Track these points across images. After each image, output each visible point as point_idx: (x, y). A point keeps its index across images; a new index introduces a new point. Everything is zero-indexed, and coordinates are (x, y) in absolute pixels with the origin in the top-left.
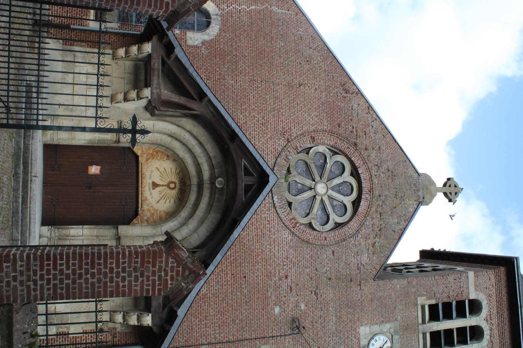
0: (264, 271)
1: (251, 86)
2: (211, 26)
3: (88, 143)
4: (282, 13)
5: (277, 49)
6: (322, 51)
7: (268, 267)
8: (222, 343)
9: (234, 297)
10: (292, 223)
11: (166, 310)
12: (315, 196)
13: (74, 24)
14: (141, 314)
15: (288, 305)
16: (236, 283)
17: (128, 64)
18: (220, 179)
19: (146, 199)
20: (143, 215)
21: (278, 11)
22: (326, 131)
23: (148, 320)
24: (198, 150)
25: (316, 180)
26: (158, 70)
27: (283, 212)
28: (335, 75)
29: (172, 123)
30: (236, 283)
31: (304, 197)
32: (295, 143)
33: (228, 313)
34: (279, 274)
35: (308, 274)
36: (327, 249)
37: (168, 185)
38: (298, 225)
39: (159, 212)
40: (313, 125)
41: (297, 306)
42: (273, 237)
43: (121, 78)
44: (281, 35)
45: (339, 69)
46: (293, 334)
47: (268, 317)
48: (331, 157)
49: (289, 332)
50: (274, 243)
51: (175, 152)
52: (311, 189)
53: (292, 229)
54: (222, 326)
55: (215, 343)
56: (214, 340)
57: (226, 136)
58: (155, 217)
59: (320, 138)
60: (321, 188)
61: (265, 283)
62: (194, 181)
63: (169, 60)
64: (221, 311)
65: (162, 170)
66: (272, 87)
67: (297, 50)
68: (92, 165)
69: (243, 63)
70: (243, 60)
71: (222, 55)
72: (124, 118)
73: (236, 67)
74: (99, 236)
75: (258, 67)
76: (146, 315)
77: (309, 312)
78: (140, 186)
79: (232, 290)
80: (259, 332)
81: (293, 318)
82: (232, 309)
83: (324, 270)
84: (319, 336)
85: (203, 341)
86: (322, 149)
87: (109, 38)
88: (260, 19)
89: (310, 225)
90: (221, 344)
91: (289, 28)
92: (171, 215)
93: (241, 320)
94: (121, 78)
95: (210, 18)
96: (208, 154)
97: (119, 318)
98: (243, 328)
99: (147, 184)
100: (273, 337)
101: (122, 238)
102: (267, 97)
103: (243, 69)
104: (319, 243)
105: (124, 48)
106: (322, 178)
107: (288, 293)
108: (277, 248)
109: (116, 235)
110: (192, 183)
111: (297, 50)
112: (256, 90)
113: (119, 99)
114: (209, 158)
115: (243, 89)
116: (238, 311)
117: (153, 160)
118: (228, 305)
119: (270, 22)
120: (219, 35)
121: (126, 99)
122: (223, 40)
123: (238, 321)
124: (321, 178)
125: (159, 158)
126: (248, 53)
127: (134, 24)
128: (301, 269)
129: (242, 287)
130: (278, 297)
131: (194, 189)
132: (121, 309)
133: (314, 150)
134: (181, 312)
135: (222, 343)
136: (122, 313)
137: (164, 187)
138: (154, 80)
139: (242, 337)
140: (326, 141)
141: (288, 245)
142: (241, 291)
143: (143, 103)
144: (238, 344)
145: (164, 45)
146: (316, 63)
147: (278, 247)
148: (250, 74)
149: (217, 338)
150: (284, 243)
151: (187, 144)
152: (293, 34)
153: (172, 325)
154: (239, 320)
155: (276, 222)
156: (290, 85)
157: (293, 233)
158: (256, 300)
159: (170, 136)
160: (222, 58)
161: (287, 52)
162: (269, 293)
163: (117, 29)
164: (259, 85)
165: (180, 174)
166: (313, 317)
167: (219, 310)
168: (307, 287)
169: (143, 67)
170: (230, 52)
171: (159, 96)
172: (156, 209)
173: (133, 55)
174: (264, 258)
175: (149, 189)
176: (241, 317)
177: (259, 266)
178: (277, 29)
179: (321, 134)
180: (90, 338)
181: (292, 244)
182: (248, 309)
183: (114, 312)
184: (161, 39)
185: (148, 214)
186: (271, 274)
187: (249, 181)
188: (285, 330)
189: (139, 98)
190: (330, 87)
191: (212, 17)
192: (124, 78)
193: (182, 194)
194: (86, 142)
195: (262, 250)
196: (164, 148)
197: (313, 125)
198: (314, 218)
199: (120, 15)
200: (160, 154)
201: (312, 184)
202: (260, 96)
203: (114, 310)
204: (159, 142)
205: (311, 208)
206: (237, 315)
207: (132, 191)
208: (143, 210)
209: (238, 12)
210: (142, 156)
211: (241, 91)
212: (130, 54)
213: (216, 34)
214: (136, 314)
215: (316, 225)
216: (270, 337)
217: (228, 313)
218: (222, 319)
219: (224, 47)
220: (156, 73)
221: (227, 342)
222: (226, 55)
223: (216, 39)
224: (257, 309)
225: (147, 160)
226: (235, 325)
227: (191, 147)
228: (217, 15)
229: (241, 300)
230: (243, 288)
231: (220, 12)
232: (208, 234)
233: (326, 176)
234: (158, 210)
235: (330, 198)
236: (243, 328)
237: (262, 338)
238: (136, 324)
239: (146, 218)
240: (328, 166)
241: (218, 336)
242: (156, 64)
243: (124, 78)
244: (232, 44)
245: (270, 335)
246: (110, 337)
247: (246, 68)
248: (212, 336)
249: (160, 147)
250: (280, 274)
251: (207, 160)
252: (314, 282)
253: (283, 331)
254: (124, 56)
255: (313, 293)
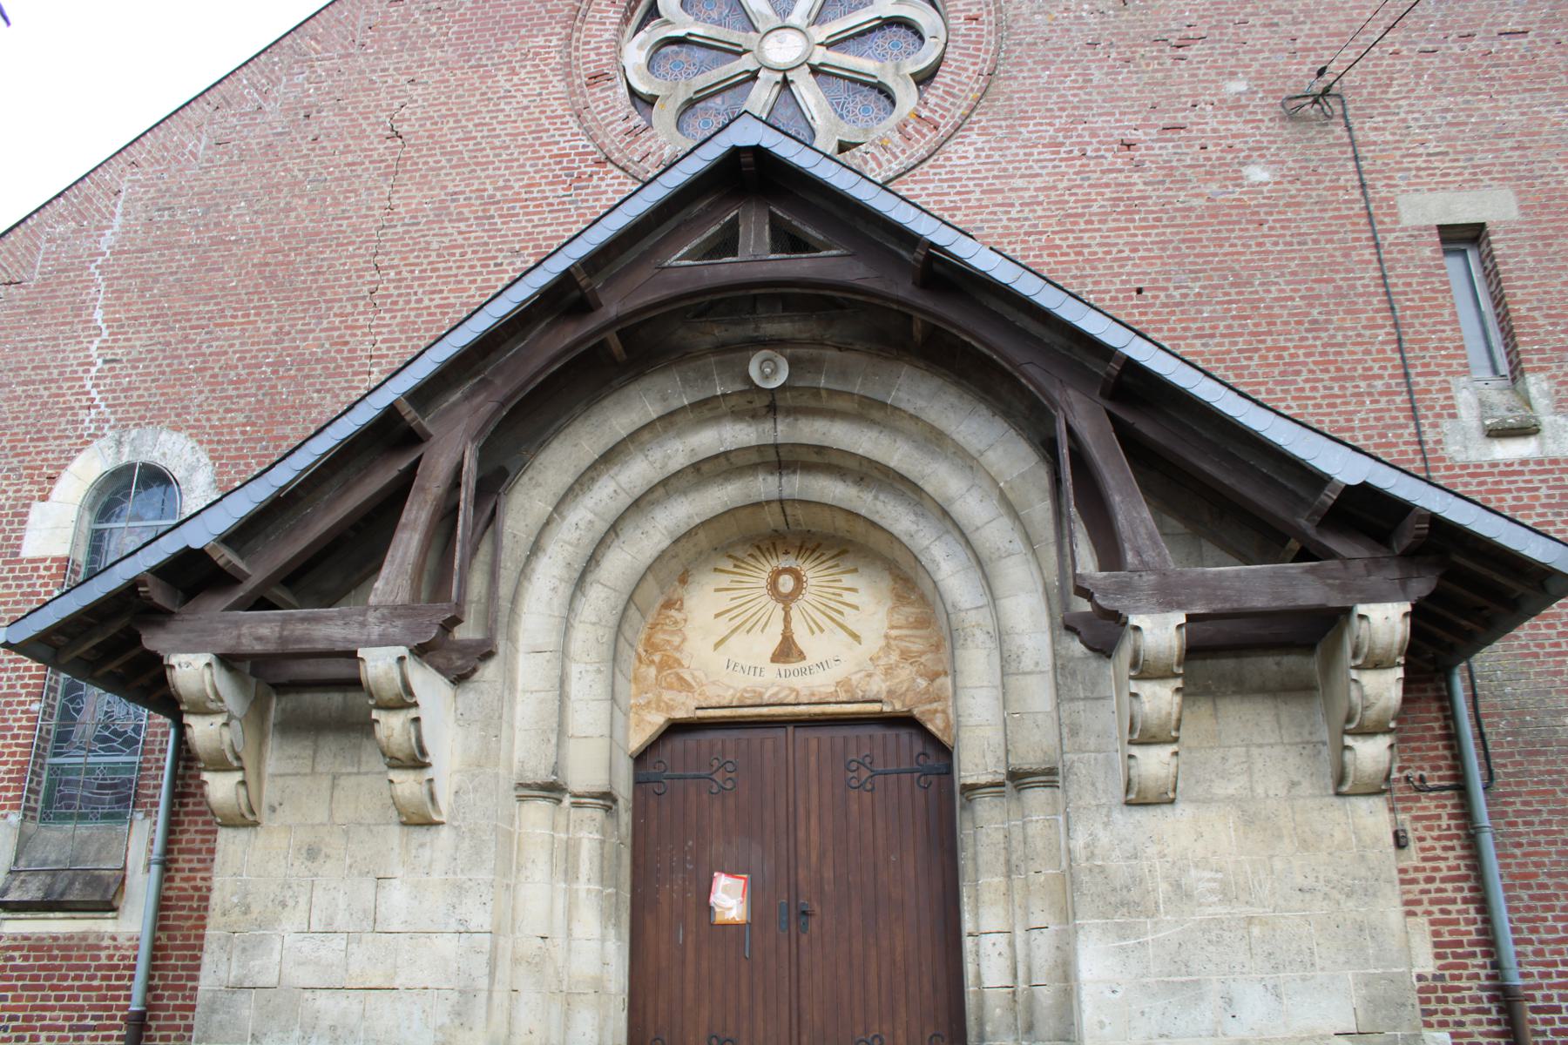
0: (1112, 225)
1: (395, 303)
2: (161, 463)
3: (617, 925)
4: (125, 214)
5: (259, 222)
6: (273, 71)
7: (1095, 209)
8: (1404, 365)
9: (1222, 330)
10: (918, 132)
11: (1332, 543)
12: (815, 70)
13: (128, 998)
14: (1355, 656)
15: (1234, 136)
16: (1166, 321)
17: (279, 758)
18: (754, 371)
19: (844, 683)
20: (910, 695)
21: (116, 229)
22: (569, 37)
23: (1385, 620)
24: (638, 472)
25: (753, 68)
26: (285, 621)
27: (880, 165)
28: (360, 23)
29: (524, 572)
30: (1166, 321)
31: (818, 104)
32: (613, 138)
33: (1285, 349)
34: (1121, 171)
35: (1113, 72)
36: (1011, 12)
37: (786, 600)
38: (925, 113)
39: (894, 633)
40: (545, 83)
41: (1237, 106)
42: (978, 195)
43: (333, 787)
44: (205, 213)
45: (341, 12)
46: (1344, 116)
47: (1288, 205)
48: (667, 22)
49: (1339, 130)
50: (1000, 191)
51: (649, 568)
52: (786, 84)
53: (942, 131)
54: (1339, 370)
55: (1410, 392)
56: (1398, 399)
57: (569, 335)
58: (916, 647)
59: (593, 57)
60: (783, 50)
61: (1159, 219)
62: (764, 486)
63: (247, 576)
64: (1282, 373)
65: (723, 627)
66: (400, 229)
67: (266, 154)
68: (710, 909)
69: (305, 339)
70: (294, 340)
71: (271, 416)
72: (502, 771)
73: (318, 361)
74: (1008, 861)
75: (321, 283)
76: (1357, 628)
77: (1256, 65)
78: (790, 709)
79: (1196, 337)
80: (1350, 236)
81: (1282, 119)
82: (1270, 333)
83: (1092, 19)
84: (1343, 27)
85: (1406, 438)
86: (635, 53)
87: (191, 851)
88: (142, 290)
89: (924, 78)
90: (1412, 371)
91: (181, 188)
92: (906, 578)
93: (1311, 299)
94: (333, 787)
95: (130, 467)
96: (649, 426)
97: (1371, 753)
98: (1339, 294)
99: (784, 681)
100: (1363, 186)
101: (1015, 763)
102: (435, 246)
103: (328, 338)
104: (993, 39)
105: (206, 776)
106: (746, 46)
107: (1189, 139)
108: (1019, 183)
109: (1001, 795)
110: (775, 496)
111: (266, 154)
112: (410, 287)
113: (416, 788)
114: (668, 422)
115: (402, 332)
116: (1276, 311)
117: (685, 662)
118: (1257, 350)
119: (155, 255)
120: (196, 431)
121: (417, 761)
122: (214, 417)
123: (1315, 312)
124: (746, 51)
125: (676, 640)
126: (269, 321)
127: (137, 759)
128: (1095, 97)
129: (1178, 299)
130: (1207, 173)
131: (796, 485)
132: (1326, 752)
133: (641, 79)
134: (1345, 469)
135: (1404, 365)
136: (1348, 741)
137: (795, 613)
138: (328, 638)
139: (1375, 294)
140: (607, 36)
141: (1006, 143)
142: (1195, 303)
143: (427, 684)
144: (1405, 309)
145: (185, 601)
146: (317, 89)
147: (1012, 176)
148: (349, 309)
149: (1388, 385)
150: (996, 158)
151: (611, 518)
152: (207, 170)
153: (1403, 508)
154: (1311, 305)
155: (918, 187)
156: (394, 171)
157: (957, 128)
158: (1227, 249)
159: (580, 583)
160: (285, 415)
161: (272, 188)
162: (1195, 202)
163: (155, 823)
164: (392, 274)
165: (739, 553)
166: (1272, 51)
167: (1277, 383)
168: (1159, 75)
169: (291, 701)
170: (260, 388)
171: (396, 612)
172: (883, 643)
173: (227, 735)
174: (1060, 223)
175: (802, 672)
176: (1298, 302)
177: (1093, 241)
178: (185, 226)
179: (580, 54)
180: (1437, 884)
181: (999, 132)
182: (1265, 275)
183: (1341, 779)
184: (157, 616)
185: (905, 673)
186: (1121, 199)
187: (759, 236)
188: (1330, 146)
189: (404, 700)
190: (405, 36)
191: (124, 460)
192: (335, 778)
193: (819, 546)
194: (612, 932)
195: (1028, 234)
196: (633, 613)
197: (545, 83)
198: (897, 67)
199: (106, 816)
200: (659, 637)
201: (768, 80)
202: (433, 270)
203: (1330, 782)
204: (606, 635)
205: (859, 82)
206: (1290, 315)
207: (813, 744)
208: (890, 692)
209: (111, 369)
210: (670, 708)
211: (409, 339)
212: (226, 747)
213: (192, 443)
214: (1354, 674)
215: (926, 57)
216: (1364, 194)
217: (1285, 349)
218: (1311, 371)
219: (241, 411)
220: (299, 629)
221: (1401, 350)
222: (273, 401)
223: (210, 442)
224: (1260, 244)
225: (684, 685)
226: (1328, 321)
227: (625, 501)
228: (119, 443)
229: (1230, 302)
230: (1185, 296)
231: (110, 433)
232: (983, 410)
233: (736, 36)
234: (887, 637)
235: (818, 19)
236: (1339, 294)
237: (1371, 223)
238: (1399, 673)
239: (922, 683)
240: (699, 30)
241: (1379, 384)
242: (260, 631)
243: (335, 778)
244: (231, 382)
245: (1357, 194)
246: (1425, 802)
247: (325, 324)
248: (1382, 405)
249: (628, 633)
250: (1119, 166)
251: (680, 434)
252: (1142, 50)
253: (1336, 150)
254: (238, 776)
255: (1180, 52)
